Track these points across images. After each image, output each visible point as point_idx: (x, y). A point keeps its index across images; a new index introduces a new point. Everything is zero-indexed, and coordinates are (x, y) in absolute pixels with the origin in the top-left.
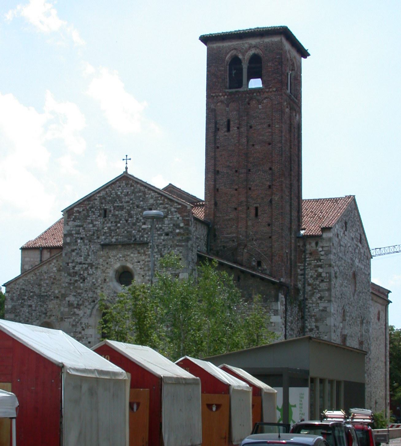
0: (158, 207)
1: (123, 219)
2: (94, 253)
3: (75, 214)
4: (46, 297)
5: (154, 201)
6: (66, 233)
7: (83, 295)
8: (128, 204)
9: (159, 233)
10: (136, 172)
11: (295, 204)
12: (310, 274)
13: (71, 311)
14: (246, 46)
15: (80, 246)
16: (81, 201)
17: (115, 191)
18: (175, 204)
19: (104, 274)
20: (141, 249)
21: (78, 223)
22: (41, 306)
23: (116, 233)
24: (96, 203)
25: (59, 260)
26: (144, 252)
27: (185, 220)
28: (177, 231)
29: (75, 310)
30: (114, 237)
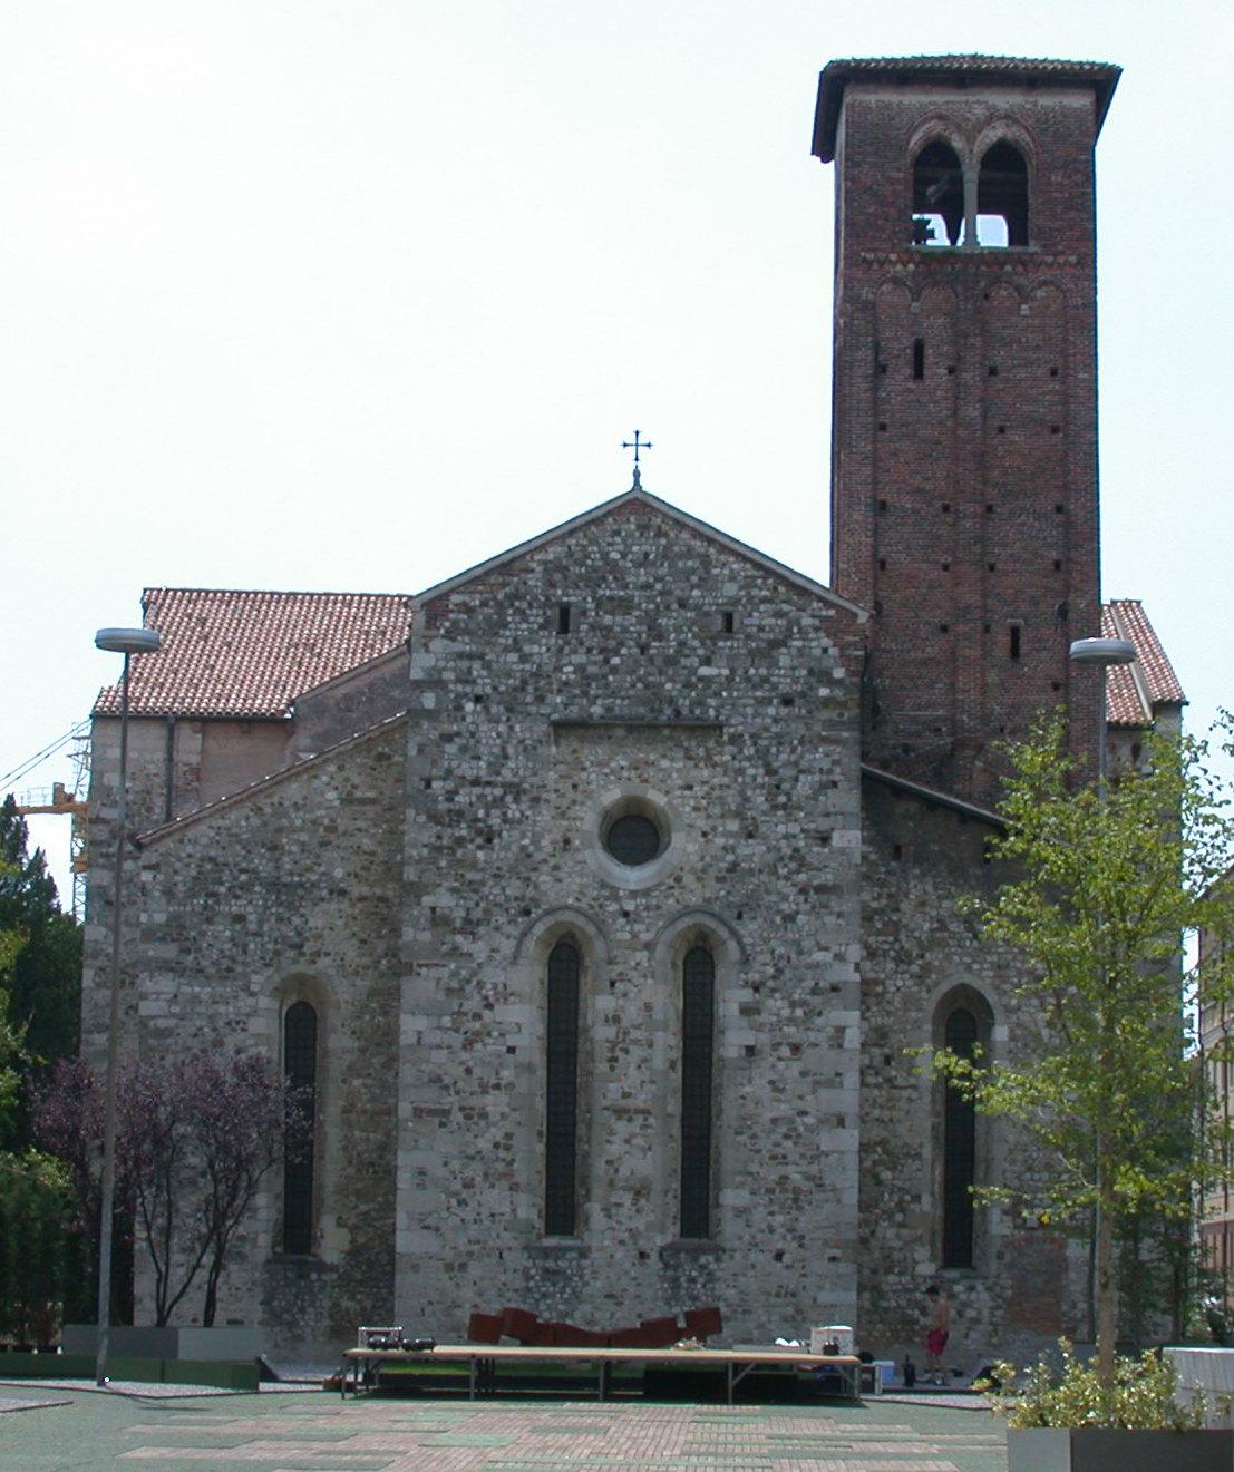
0: (753, 610)
1: (632, 643)
2: (525, 749)
3: (452, 616)
4: (300, 892)
5: (741, 588)
6: (261, 1298)
7: (486, 890)
8: (648, 593)
9: (759, 694)
13: (443, 943)
14: (979, 111)
15: (473, 723)
16: (479, 571)
17: (598, 545)
18: (815, 605)
19: (565, 823)
20: (698, 746)
21: (464, 645)
22: (280, 920)
23: (607, 685)
24: (531, 583)
25: (348, 766)
26: (709, 757)
27: (848, 658)
28: (824, 692)
29: (459, 938)
30: (599, 702)
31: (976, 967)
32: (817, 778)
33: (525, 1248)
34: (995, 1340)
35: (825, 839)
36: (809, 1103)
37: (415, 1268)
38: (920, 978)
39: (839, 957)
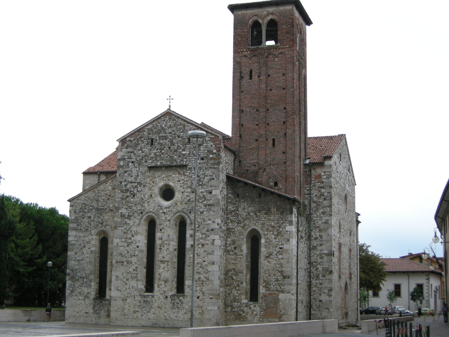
4: (103, 210)
6: (92, 307)
7: (133, 208)
10: (176, 109)
11: (303, 138)
12: (315, 194)
14: (265, 13)
21: (130, 150)
22: (98, 217)
23: (161, 158)
26: (184, 173)
28: (211, 156)
29: (127, 220)
31: (257, 224)
32: (209, 177)
33: (140, 295)
34: (261, 320)
35: (211, 193)
36: (206, 259)
37: (115, 300)
38: (243, 227)
39: (214, 222)
